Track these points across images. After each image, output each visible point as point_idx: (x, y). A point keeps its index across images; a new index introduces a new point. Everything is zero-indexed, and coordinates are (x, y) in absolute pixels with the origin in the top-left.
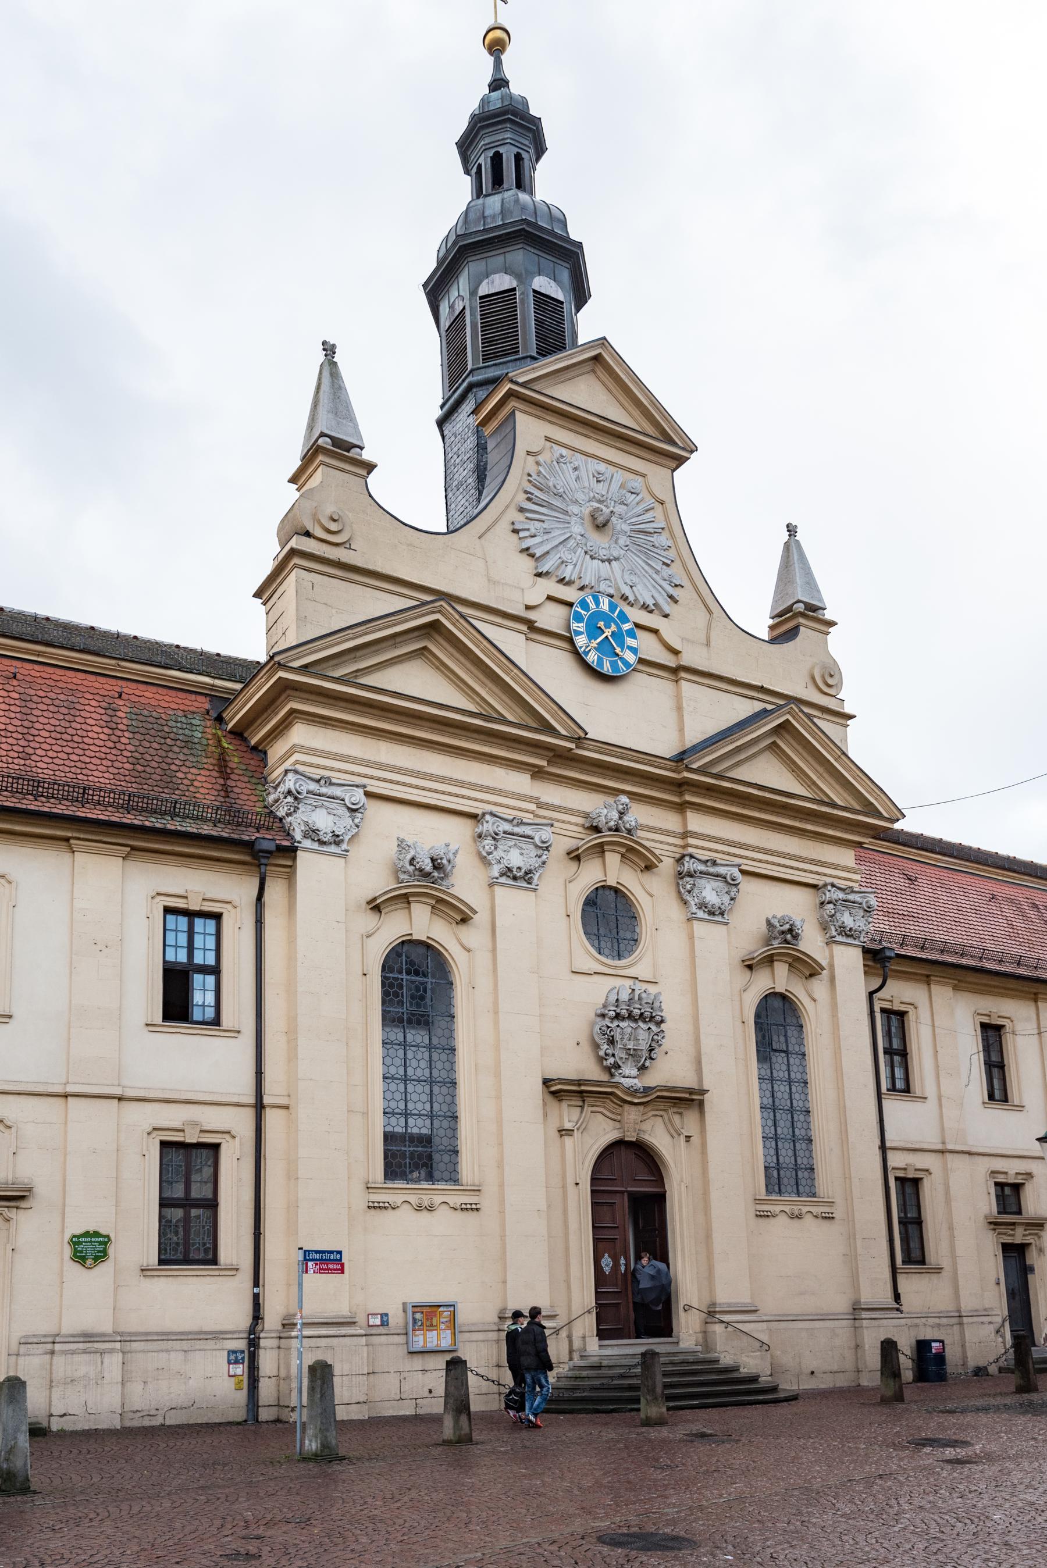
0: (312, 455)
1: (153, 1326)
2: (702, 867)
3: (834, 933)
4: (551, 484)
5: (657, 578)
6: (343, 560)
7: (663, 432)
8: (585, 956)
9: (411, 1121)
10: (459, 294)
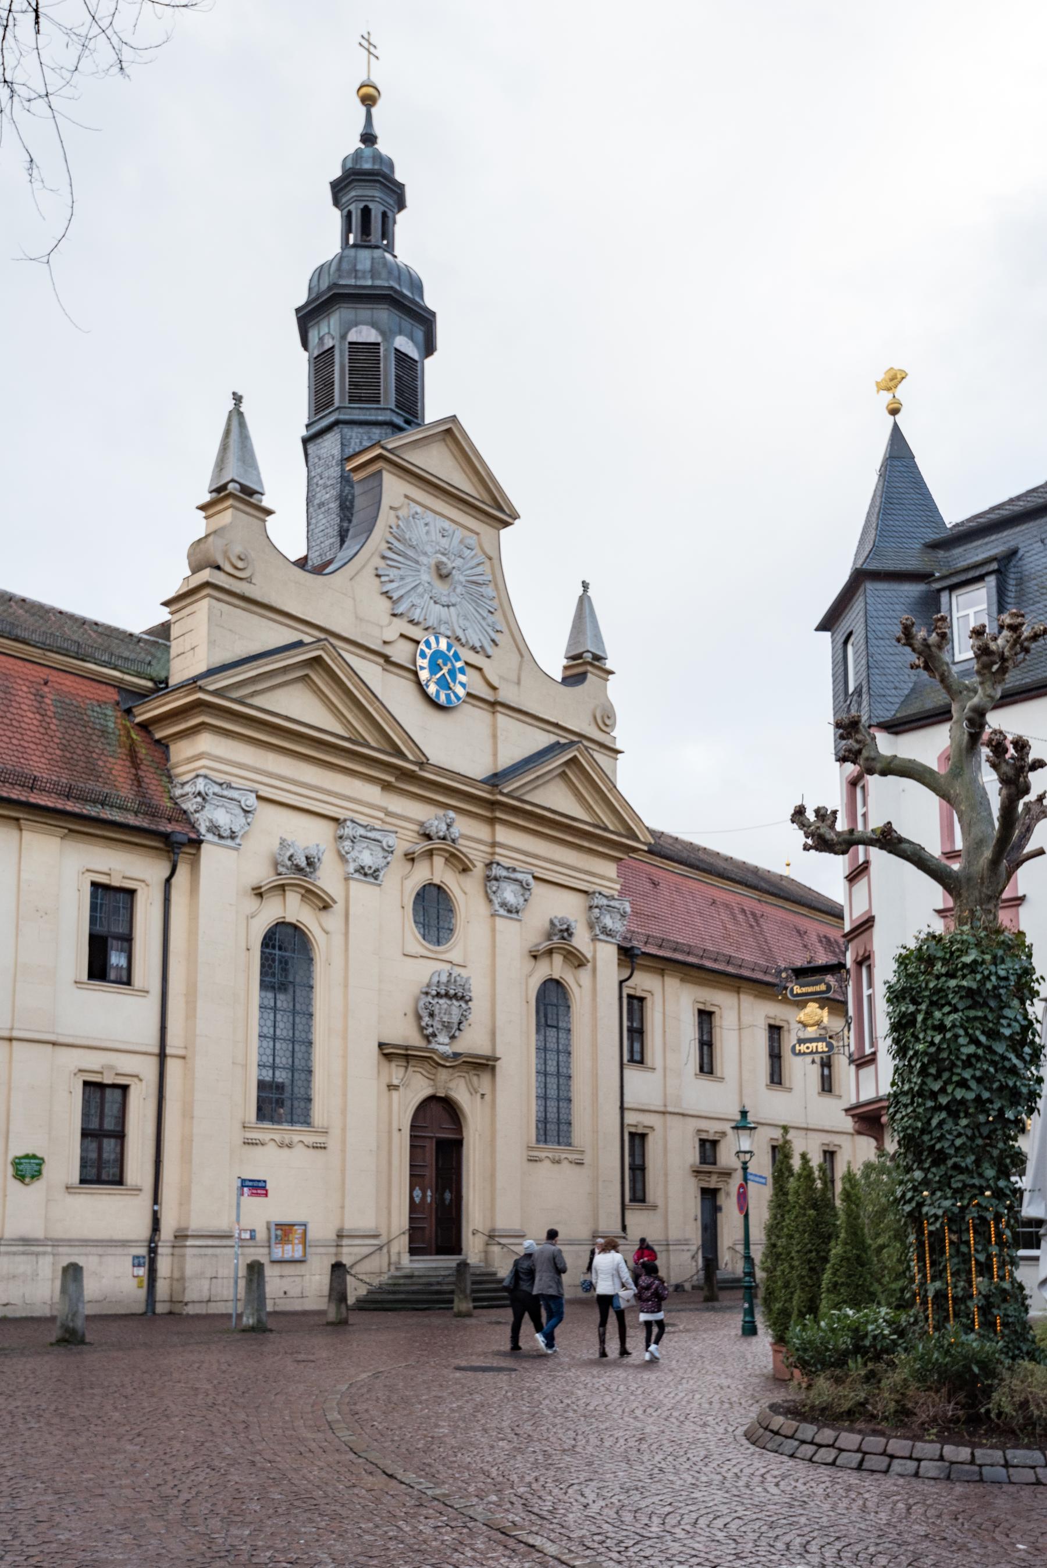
0: (220, 491)
1: (73, 1234)
2: (504, 873)
3: (598, 932)
4: (407, 537)
5: (484, 623)
6: (247, 594)
7: (495, 499)
8: (414, 941)
9: (277, 1073)
10: (327, 330)
